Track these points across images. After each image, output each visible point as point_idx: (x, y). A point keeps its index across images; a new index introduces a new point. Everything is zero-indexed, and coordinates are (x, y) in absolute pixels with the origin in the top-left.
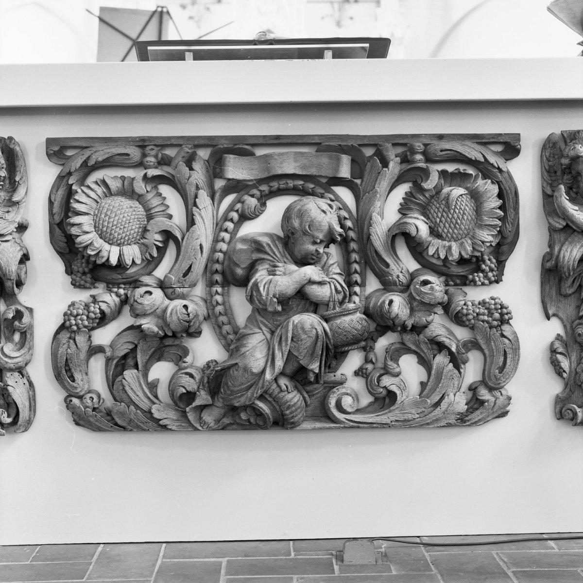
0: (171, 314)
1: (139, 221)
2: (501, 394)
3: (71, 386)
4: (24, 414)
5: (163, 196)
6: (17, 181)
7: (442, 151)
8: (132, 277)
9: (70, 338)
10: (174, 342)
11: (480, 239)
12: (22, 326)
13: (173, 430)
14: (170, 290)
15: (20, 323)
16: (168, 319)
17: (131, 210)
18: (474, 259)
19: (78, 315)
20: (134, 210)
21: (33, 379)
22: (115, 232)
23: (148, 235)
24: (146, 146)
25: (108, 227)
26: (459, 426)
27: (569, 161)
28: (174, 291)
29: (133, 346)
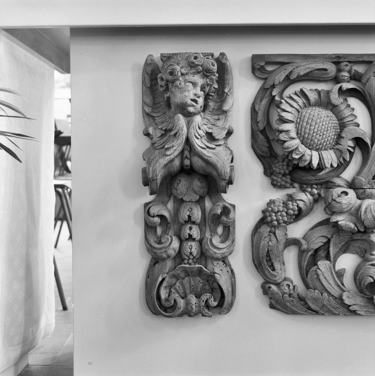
0: (365, 212)
1: (334, 129)
3: (271, 275)
4: (228, 298)
5: (351, 107)
6: (226, 92)
8: (324, 179)
9: (270, 232)
10: (362, 236)
12: (229, 221)
13: (361, 315)
14: (361, 191)
15: (227, 218)
16: (363, 217)
17: (328, 119)
19: (278, 212)
20: (331, 119)
21: (233, 267)
22: (315, 138)
23: (343, 142)
24: (340, 63)
25: (309, 134)
28: (364, 191)
29: (326, 240)
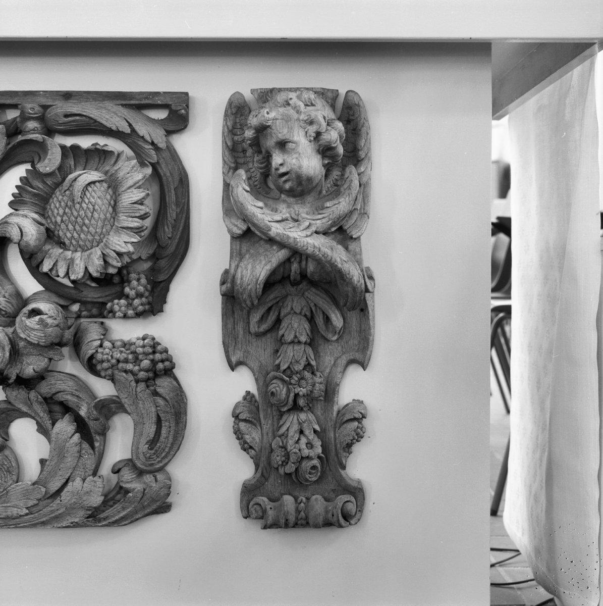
2: (156, 480)
7: (66, 116)
11: (114, 249)
18: (117, 278)
26: (91, 526)
27: (254, 133)
